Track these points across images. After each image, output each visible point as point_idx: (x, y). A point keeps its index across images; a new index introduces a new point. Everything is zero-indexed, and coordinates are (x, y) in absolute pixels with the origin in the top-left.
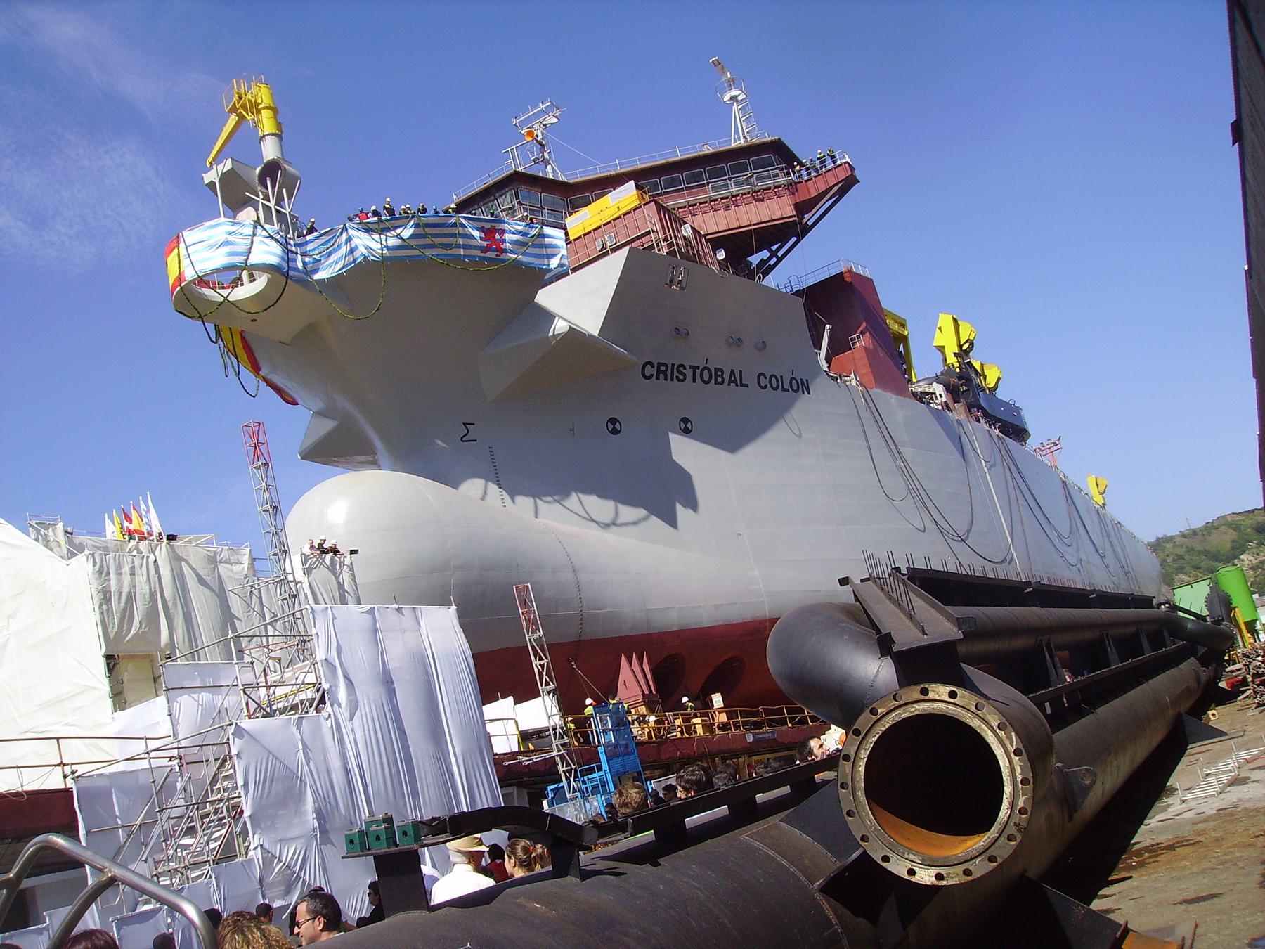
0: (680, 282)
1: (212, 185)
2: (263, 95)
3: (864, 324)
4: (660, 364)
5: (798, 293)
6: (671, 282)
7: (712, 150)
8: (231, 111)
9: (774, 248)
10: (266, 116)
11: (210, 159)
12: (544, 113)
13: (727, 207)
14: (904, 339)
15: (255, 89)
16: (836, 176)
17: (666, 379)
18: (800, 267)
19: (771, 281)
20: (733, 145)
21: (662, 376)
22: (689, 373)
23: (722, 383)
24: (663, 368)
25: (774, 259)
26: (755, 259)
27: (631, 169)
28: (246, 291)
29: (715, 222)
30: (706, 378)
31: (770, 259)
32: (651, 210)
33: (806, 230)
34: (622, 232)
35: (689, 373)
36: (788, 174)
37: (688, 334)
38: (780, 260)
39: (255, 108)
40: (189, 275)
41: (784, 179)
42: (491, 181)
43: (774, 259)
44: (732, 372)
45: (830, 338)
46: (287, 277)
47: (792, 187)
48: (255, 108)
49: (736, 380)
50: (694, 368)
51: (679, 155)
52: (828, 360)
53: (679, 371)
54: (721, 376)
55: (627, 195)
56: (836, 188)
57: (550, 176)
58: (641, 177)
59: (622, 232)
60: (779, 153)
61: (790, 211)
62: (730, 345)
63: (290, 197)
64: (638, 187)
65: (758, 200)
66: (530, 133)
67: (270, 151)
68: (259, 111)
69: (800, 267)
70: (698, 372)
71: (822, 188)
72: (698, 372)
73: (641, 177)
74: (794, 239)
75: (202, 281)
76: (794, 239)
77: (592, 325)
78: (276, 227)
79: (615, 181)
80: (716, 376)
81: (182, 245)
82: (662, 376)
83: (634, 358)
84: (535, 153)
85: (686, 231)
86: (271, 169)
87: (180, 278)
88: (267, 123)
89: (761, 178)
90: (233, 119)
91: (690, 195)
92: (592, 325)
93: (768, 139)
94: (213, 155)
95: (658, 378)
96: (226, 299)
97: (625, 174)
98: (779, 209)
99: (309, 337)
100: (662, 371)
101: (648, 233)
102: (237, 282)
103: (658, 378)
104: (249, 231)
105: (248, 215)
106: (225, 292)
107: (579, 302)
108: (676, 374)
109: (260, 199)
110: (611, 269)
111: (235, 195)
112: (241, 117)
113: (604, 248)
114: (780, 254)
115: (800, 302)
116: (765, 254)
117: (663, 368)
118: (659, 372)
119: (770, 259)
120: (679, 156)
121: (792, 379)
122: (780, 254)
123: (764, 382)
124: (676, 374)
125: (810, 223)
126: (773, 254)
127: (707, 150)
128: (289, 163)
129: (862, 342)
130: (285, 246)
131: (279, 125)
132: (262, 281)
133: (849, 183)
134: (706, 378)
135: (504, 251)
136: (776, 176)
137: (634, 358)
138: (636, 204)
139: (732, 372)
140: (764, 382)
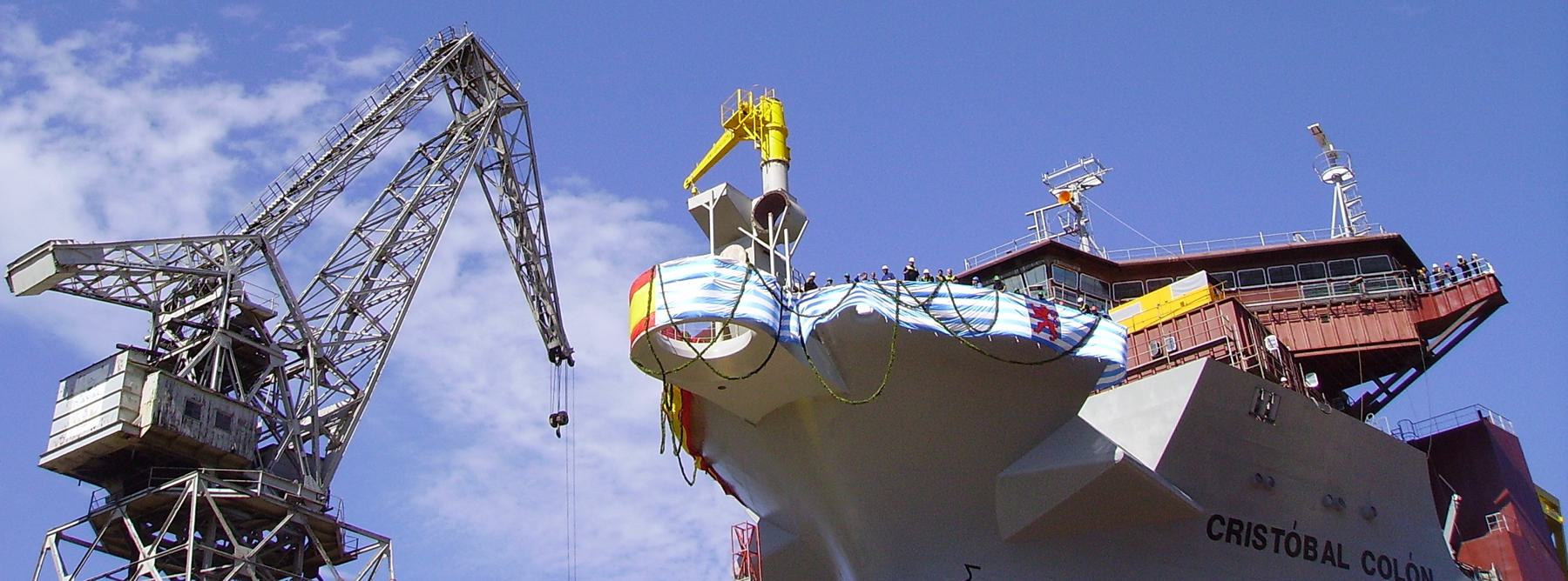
0: (1268, 413)
1: (700, 213)
2: (770, 110)
3: (1506, 491)
4: (1232, 521)
5: (1420, 444)
6: (1257, 410)
7: (1305, 242)
8: (727, 127)
9: (1384, 380)
10: (774, 138)
11: (690, 179)
12: (1085, 170)
13: (1324, 318)
14: (1558, 528)
15: (763, 105)
16: (1474, 291)
17: (1239, 543)
18: (1419, 410)
19: (1383, 421)
20: (1334, 238)
21: (1234, 537)
22: (1270, 538)
23: (1314, 558)
24: (1236, 527)
25: (1384, 395)
26: (1355, 393)
27: (1242, 250)
28: (720, 349)
29: (1307, 336)
30: (1293, 548)
31: (1378, 393)
32: (1228, 311)
33: (1431, 359)
34: (1185, 335)
35: (1270, 538)
36: (1410, 282)
37: (1272, 483)
38: (1391, 396)
39: (763, 128)
40: (661, 319)
41: (1403, 289)
42: (1016, 251)
43: (1384, 395)
44: (1329, 543)
45: (1458, 520)
46: (777, 338)
47: (1414, 301)
48: (763, 128)
49: (1333, 556)
50: (1278, 532)
51: (1263, 244)
52: (1455, 543)
53: (1257, 534)
54: (1314, 549)
55: (1194, 289)
56: (1475, 308)
57: (1086, 250)
58: (1220, 269)
59: (1185, 335)
60: (1398, 253)
61: (1410, 333)
62: (1326, 506)
63: (791, 240)
64: (1211, 280)
65: (1368, 312)
66: (1065, 195)
67: (772, 180)
68: (766, 131)
69: (1419, 410)
70: (1283, 538)
71: (1456, 305)
72: (1283, 538)
73: (1220, 269)
74: (1413, 371)
75: (671, 329)
76: (1413, 371)
77: (1150, 458)
78: (773, 275)
79: (1181, 268)
80: (1307, 547)
81: (656, 280)
82: (1234, 537)
83: (1200, 509)
84: (1069, 221)
85: (1271, 343)
86: (773, 203)
87: (648, 320)
88: (773, 146)
89: (1374, 285)
90: (728, 136)
91: (1275, 297)
92: (1150, 458)
93: (1382, 233)
94: (694, 174)
95: (1228, 540)
96: (699, 356)
97: (1190, 261)
98: (1396, 327)
99: (782, 419)
100: (1236, 531)
101: (1223, 341)
102: (707, 337)
103: (1228, 540)
104: (741, 274)
105: (734, 252)
106: (700, 347)
107: (1137, 422)
108: (1253, 537)
109: (754, 236)
110: (1182, 381)
111: (725, 227)
112: (740, 135)
113: (1160, 354)
114: (1391, 389)
115: (1422, 457)
116: (1371, 387)
117: (1236, 527)
118: (1230, 531)
119: (1378, 393)
120: (1263, 246)
121: (1410, 565)
122: (1391, 389)
123: (1371, 564)
124: (1253, 537)
125: (1435, 352)
126: (1383, 388)
127: (1299, 240)
128: (795, 200)
129: (1503, 521)
130: (779, 299)
131: (787, 150)
132: (741, 340)
133: (1495, 301)
134: (1293, 548)
135: (1058, 335)
136: (1393, 283)
137: (1200, 509)
138: (1208, 301)
139: (1329, 543)
140: (1371, 564)
